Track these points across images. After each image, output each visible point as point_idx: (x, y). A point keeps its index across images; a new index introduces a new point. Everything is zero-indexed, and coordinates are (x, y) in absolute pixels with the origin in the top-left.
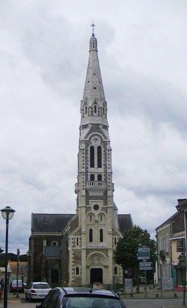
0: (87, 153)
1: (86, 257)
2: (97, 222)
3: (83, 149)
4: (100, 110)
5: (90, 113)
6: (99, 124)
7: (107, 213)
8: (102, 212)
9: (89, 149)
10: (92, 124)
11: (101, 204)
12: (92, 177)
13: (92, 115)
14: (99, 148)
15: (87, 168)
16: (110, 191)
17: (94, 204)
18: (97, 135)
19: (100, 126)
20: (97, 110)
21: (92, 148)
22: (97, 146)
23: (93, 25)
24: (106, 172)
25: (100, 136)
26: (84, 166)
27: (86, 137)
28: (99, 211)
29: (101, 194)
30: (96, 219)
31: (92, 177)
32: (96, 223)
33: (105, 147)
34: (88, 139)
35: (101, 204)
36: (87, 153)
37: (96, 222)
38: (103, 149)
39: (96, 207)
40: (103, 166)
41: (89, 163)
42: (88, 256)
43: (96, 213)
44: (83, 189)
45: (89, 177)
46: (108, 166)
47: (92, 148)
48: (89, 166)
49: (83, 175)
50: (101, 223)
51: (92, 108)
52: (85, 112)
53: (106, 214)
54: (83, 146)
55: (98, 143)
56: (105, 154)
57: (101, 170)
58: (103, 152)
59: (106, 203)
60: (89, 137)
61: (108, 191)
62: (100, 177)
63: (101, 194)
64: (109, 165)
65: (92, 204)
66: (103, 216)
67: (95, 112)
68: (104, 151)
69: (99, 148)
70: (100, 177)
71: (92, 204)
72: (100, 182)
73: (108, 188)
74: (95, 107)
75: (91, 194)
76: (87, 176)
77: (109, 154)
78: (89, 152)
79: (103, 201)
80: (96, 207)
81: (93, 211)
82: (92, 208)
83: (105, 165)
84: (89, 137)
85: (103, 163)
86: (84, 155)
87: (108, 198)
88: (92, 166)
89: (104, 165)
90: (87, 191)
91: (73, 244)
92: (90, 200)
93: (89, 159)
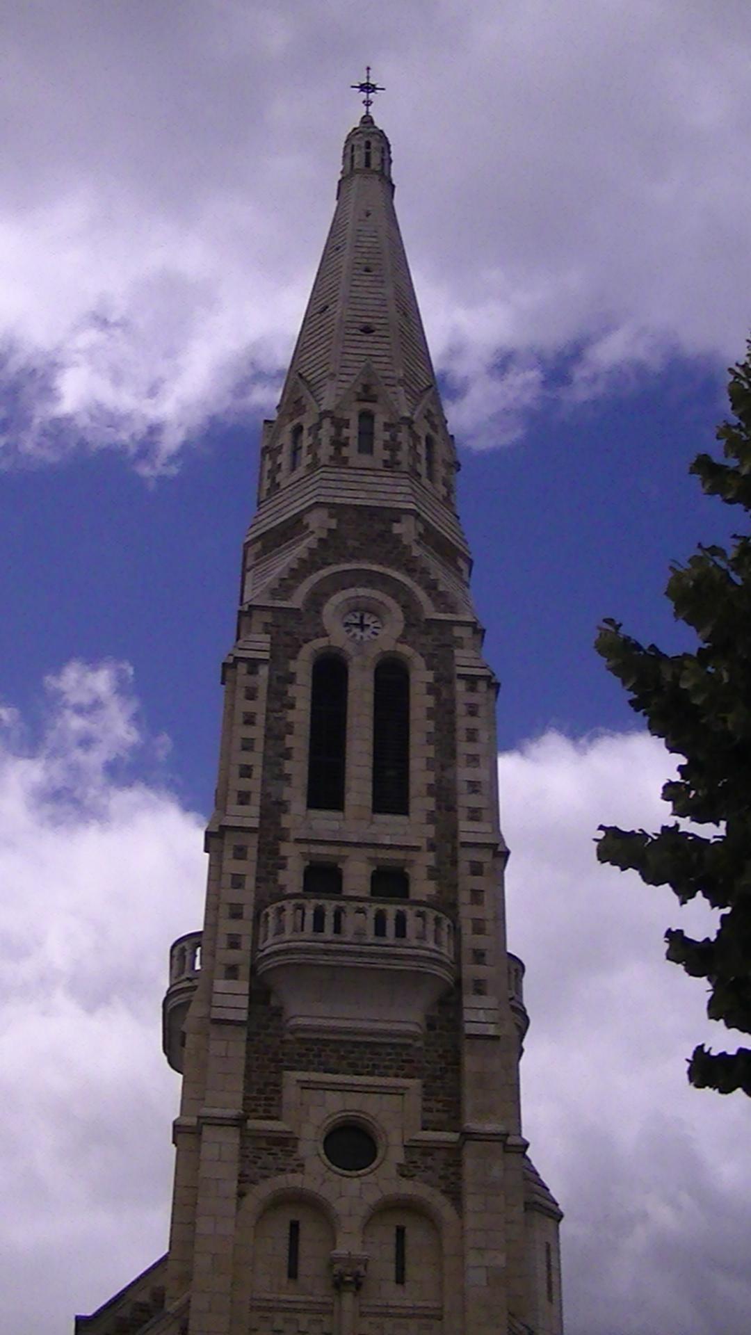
0: (279, 696)
1: (241, 1195)
2: (347, 1280)
3: (253, 665)
4: (403, 436)
5: (326, 451)
6: (396, 515)
7: (456, 1197)
8: (407, 1188)
9: (302, 667)
10: (336, 510)
11: (395, 1113)
12: (323, 877)
13: (339, 461)
14: (392, 678)
15: (273, 809)
16: (489, 1001)
17: (334, 1106)
18: (371, 579)
19: (397, 529)
20: (381, 436)
21: (331, 672)
22: (374, 652)
23: (367, 88)
24: (446, 843)
25: (397, 590)
26: (253, 785)
27: (284, 587)
28: (383, 1180)
29: (405, 1017)
30: (348, 1245)
31: (323, 877)
32: (348, 1300)
33: (440, 658)
34: (297, 600)
35: (395, 1113)
36: (279, 696)
37: (339, 1284)
38: (421, 676)
39: (351, 1144)
40: (421, 803)
41: (298, 768)
42: (251, 1202)
43: (352, 1194)
44: (232, 972)
45: (292, 878)
46: (466, 800)
47: (331, 672)
48: (296, 795)
49: (240, 853)
50: (391, 1294)
51: (340, 424)
52: (284, 459)
53: (448, 1213)
54: (259, 643)
55: (387, 634)
56: (444, 713)
57: (410, 829)
58: (420, 702)
59: (445, 1099)
60: (304, 588)
61: (469, 1000)
62: (390, 881)
63: (405, 1017)
64: (474, 786)
65: (311, 1109)
66: (416, 1236)
67: (366, 444)
68: (431, 690)
69: (392, 678)
70: (390, 881)
71: (311, 1109)
72: (391, 910)
73: (470, 971)
74: (367, 417)
75: (307, 1012)
76: (271, 862)
77: (237, 881)
78: (302, 693)
79: (414, 1084)
80: (351, 1144)
81: (314, 1172)
82: (310, 1147)
83: (444, 795)
84: (304, 588)
85: (420, 776)
86: (259, 707)
87: (470, 1063)
88: (326, 790)
89: (431, 790)
90: (260, 994)
91: (386, 455)
92: (292, 1077)
93: (299, 742)
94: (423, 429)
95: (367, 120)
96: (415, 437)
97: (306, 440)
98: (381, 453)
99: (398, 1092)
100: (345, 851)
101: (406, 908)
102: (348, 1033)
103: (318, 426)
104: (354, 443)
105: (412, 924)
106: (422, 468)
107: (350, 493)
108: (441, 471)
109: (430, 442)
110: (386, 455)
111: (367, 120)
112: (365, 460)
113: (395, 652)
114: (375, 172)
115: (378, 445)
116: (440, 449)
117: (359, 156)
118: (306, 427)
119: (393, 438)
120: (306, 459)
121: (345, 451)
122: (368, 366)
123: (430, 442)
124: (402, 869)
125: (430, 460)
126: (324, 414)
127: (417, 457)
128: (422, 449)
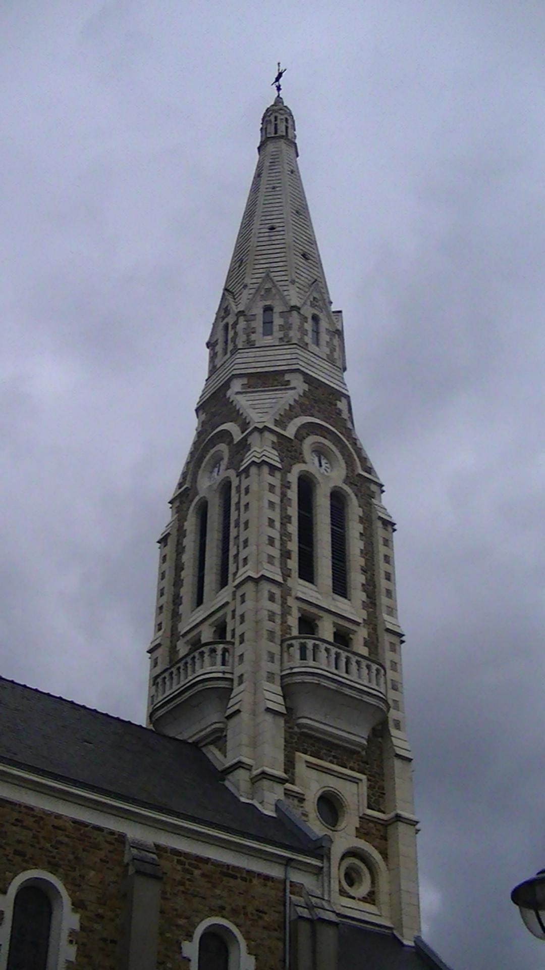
11: (354, 795)
20: (278, 321)
62: (342, 638)
69: (338, 499)
70: (342, 638)
75: (313, 717)
94: (308, 311)
95: (279, 100)
96: (305, 319)
97: (231, 334)
98: (278, 334)
99: (356, 781)
100: (321, 613)
101: (341, 651)
102: (348, 742)
103: (236, 323)
104: (260, 330)
105: (354, 667)
106: (308, 339)
107: (323, 375)
108: (324, 337)
109: (315, 318)
110: (281, 334)
111: (279, 100)
112: (268, 340)
113: (314, 475)
114: (282, 137)
115: (276, 328)
116: (324, 324)
117: (271, 129)
118: (230, 324)
119: (286, 322)
120: (230, 347)
121: (253, 337)
122: (268, 275)
123: (315, 318)
124: (314, 620)
125: (317, 332)
126: (241, 313)
127: (304, 332)
128: (309, 326)
